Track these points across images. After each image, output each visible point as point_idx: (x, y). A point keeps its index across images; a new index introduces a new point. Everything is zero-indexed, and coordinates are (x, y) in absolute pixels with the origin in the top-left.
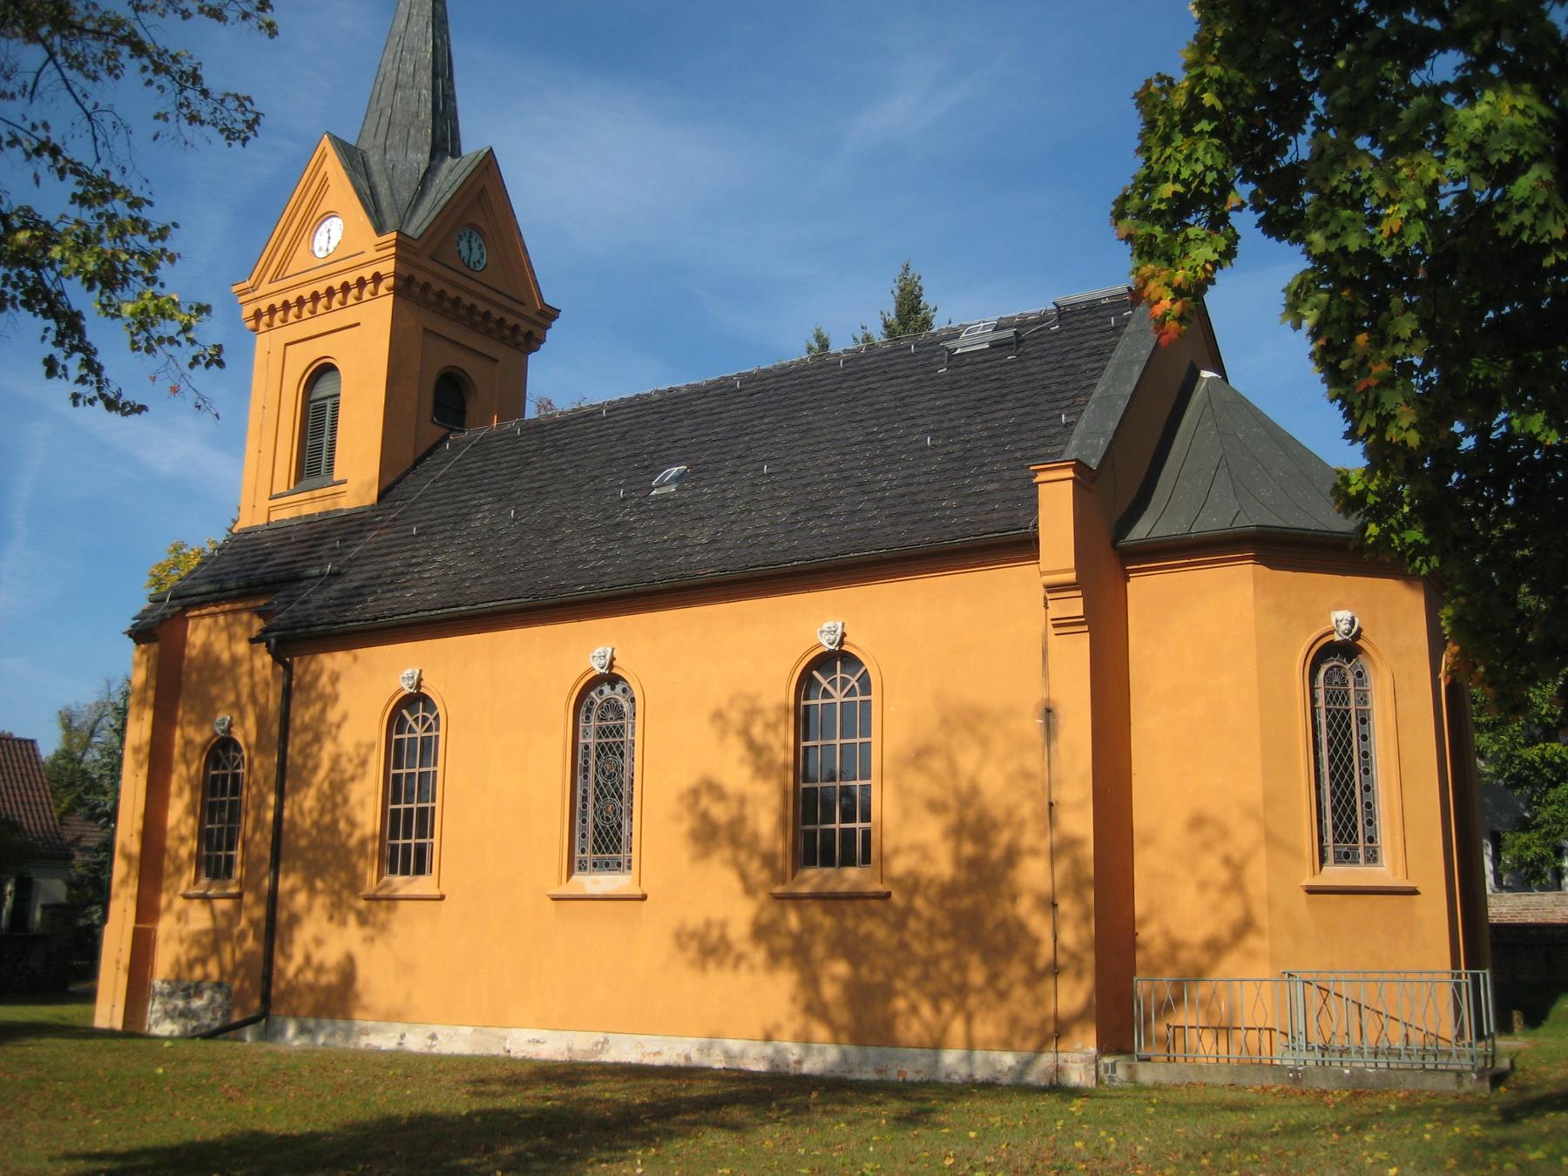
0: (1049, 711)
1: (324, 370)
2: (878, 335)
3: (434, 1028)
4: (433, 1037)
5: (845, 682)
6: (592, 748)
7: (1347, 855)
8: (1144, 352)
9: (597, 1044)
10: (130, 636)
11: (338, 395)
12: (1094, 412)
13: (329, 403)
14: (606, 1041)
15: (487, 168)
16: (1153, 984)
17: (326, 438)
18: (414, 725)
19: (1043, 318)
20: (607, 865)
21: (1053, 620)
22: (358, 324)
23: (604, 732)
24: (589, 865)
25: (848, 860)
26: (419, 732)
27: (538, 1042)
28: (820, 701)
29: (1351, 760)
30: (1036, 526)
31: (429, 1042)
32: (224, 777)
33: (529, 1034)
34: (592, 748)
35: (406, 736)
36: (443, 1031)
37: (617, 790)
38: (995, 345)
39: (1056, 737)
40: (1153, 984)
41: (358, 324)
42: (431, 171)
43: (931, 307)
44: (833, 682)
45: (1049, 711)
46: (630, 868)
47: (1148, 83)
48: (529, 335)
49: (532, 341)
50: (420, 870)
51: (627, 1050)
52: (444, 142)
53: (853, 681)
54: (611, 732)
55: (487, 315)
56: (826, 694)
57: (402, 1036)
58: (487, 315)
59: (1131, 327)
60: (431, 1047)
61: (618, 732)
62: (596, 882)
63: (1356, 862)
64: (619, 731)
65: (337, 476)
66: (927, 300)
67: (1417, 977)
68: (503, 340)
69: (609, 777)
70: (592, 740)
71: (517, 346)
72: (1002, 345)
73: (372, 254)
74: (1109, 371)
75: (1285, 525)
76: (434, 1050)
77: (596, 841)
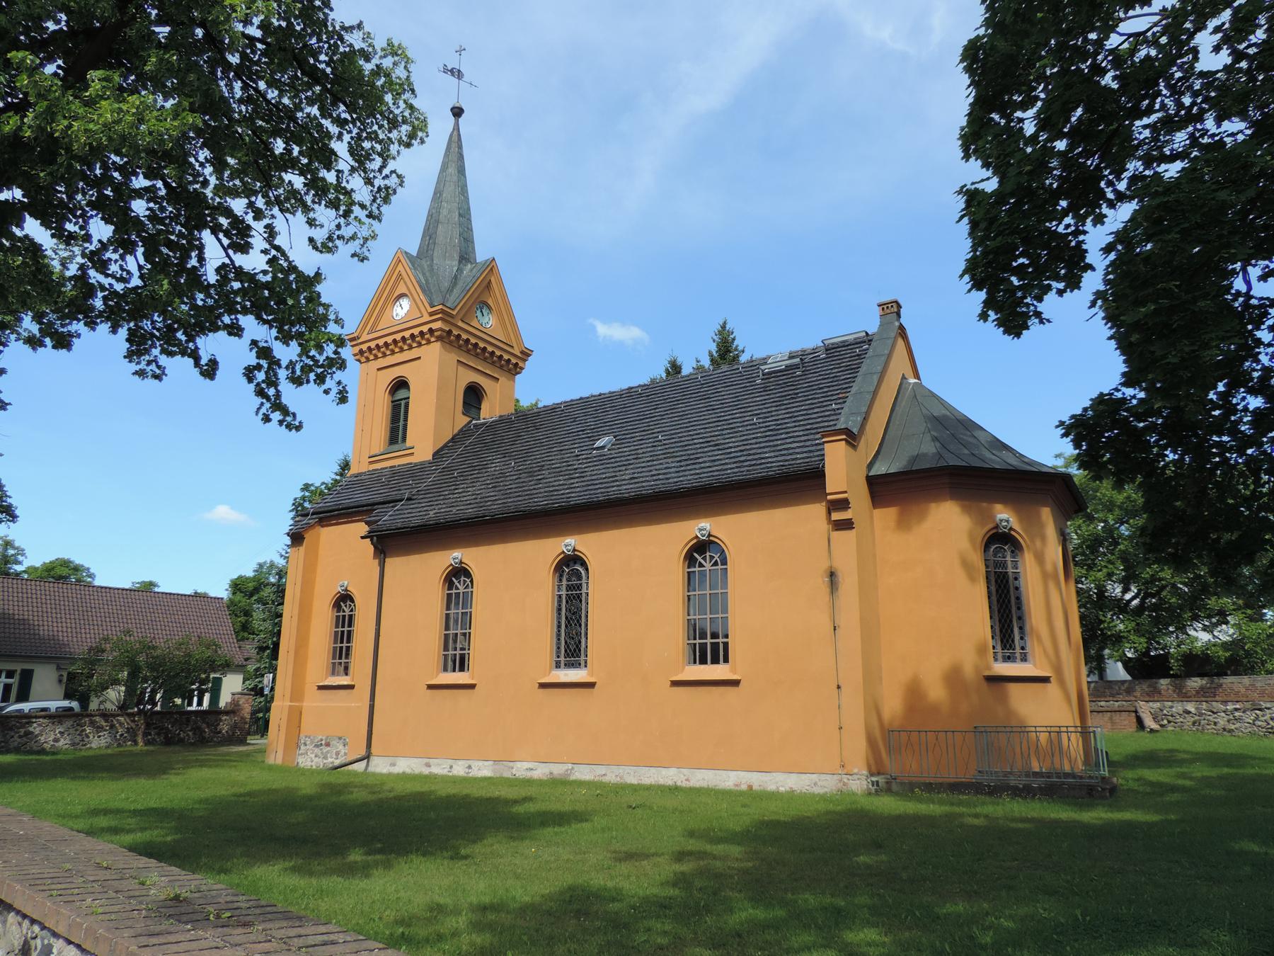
0: (832, 574)
1: (401, 384)
2: (706, 363)
3: (470, 762)
4: (470, 767)
5: (712, 557)
6: (564, 597)
7: (1009, 658)
8: (879, 368)
9: (567, 770)
10: (288, 535)
11: (408, 398)
12: (852, 401)
13: (403, 403)
14: (573, 768)
15: (491, 269)
16: (1050, 735)
17: (401, 423)
18: (458, 585)
19: (814, 351)
20: (573, 665)
22: (419, 358)
23: (570, 588)
24: (562, 664)
25: (715, 661)
26: (347, 613)
27: (532, 769)
28: (697, 569)
29: (1009, 601)
30: (823, 467)
31: (467, 770)
32: (344, 616)
33: (526, 765)
34: (564, 597)
35: (454, 591)
36: (475, 764)
37: (569, 622)
38: (788, 368)
39: (837, 589)
40: (1050, 735)
41: (419, 358)
42: (460, 270)
43: (740, 348)
44: (704, 559)
45: (832, 574)
46: (586, 666)
47: (312, 485)
50: (462, 669)
51: (584, 773)
52: (466, 256)
53: (716, 557)
54: (574, 588)
55: (493, 353)
56: (701, 565)
57: (451, 767)
58: (493, 353)
59: (870, 353)
60: (468, 773)
61: (578, 587)
62: (566, 675)
63: (1014, 661)
64: (579, 587)
65: (408, 444)
66: (739, 343)
67: (1003, 729)
68: (501, 367)
69: (573, 614)
70: (564, 593)
71: (509, 371)
72: (9, 656)
73: (427, 318)
74: (859, 379)
75: (967, 465)
76: (471, 775)
77: (566, 651)
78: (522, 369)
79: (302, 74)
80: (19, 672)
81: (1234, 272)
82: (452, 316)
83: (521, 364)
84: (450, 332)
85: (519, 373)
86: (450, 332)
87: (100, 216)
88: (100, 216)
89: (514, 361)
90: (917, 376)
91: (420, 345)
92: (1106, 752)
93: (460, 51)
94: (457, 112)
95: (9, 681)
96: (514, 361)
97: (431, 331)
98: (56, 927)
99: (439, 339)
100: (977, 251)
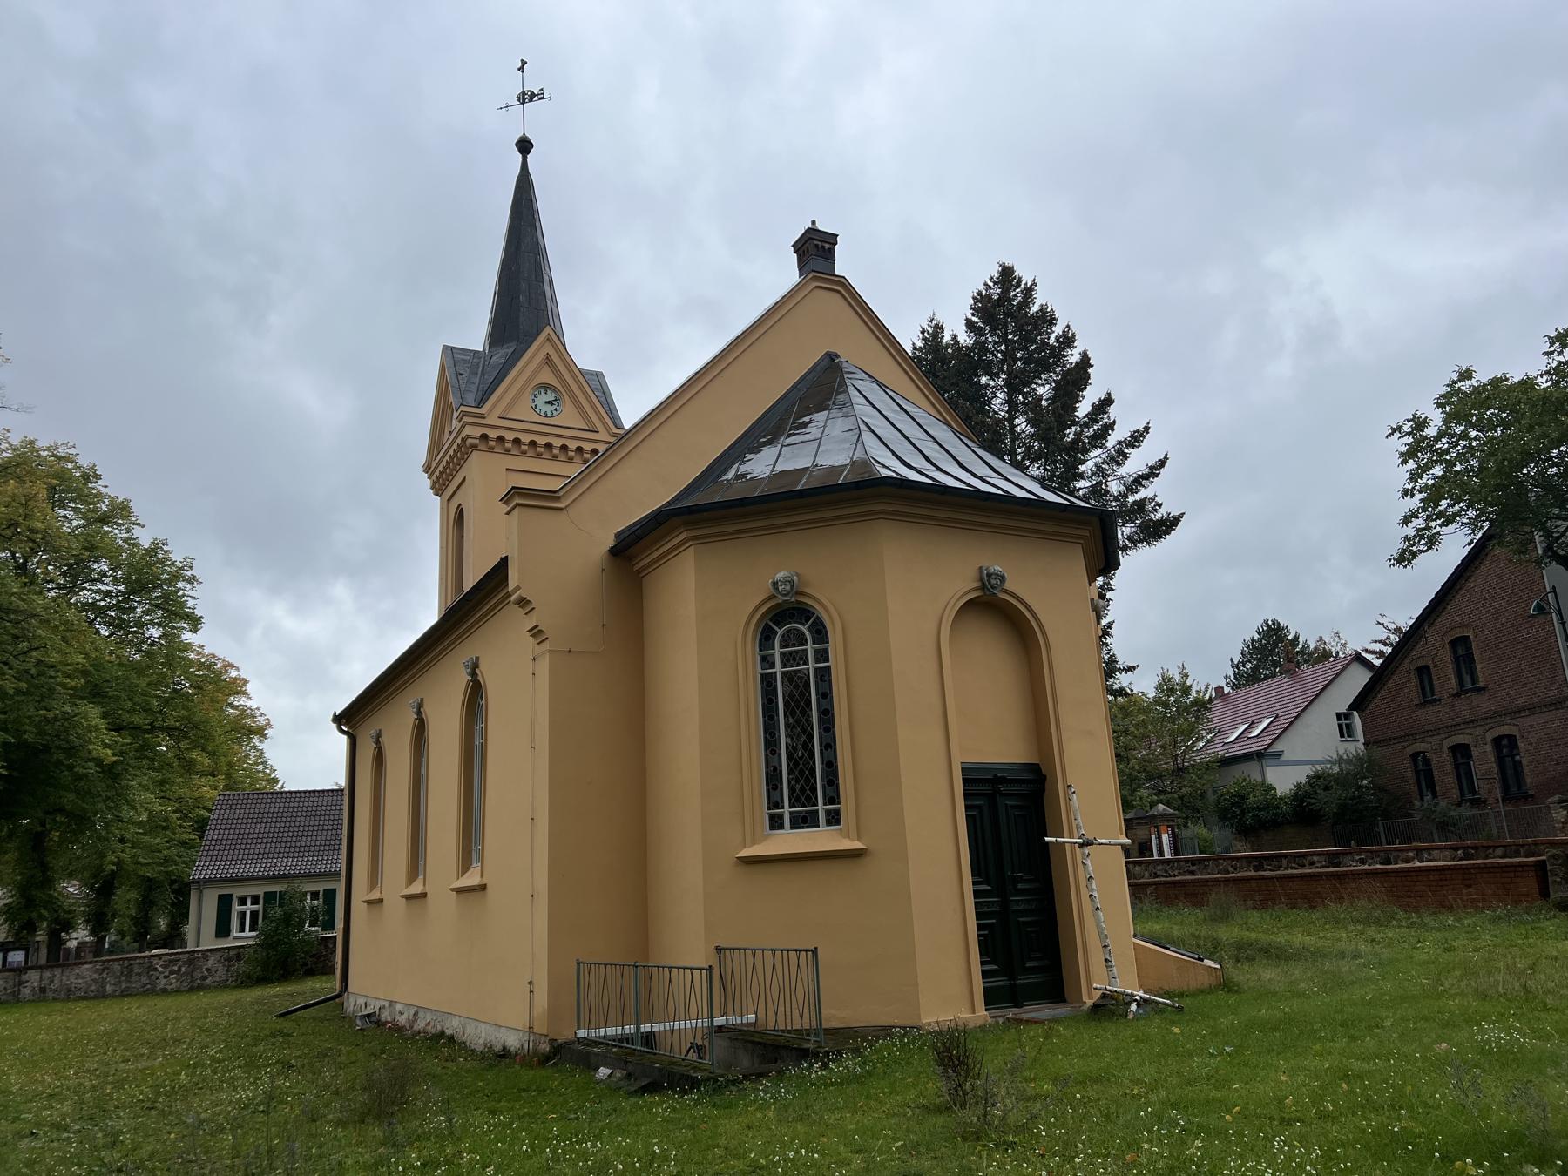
21: (529, 631)
80: (262, 896)
82: (482, 417)
94: (524, 146)
95: (255, 907)
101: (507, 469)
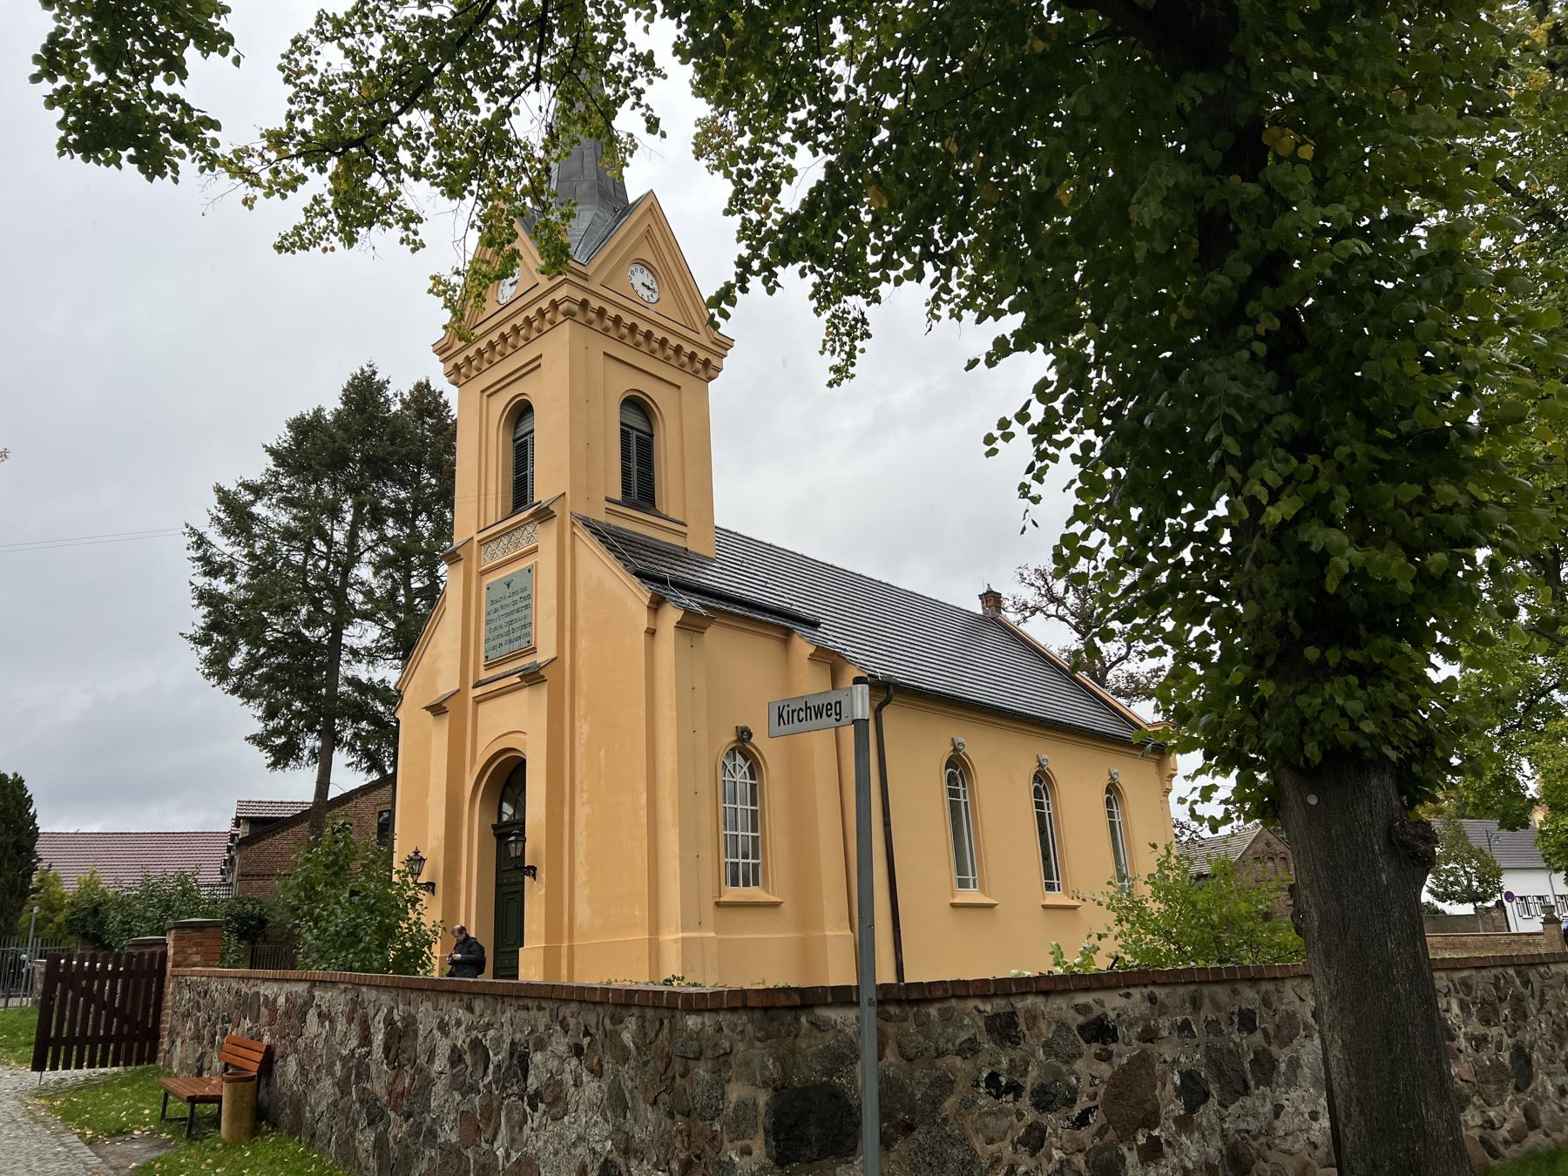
48: (706, 363)
49: (708, 370)
78: (719, 370)
79: (1232, 609)
81: (1109, 458)
82: (585, 277)
83: (714, 361)
84: (584, 304)
85: (711, 379)
86: (584, 304)
87: (832, 158)
88: (832, 158)
89: (702, 355)
90: (1073, 482)
91: (541, 332)
92: (539, 366)
93: (1154, 846)
96: (702, 355)
97: (554, 305)
98: (294, 834)
99: (569, 314)
100: (1114, 464)
101: (605, 354)
